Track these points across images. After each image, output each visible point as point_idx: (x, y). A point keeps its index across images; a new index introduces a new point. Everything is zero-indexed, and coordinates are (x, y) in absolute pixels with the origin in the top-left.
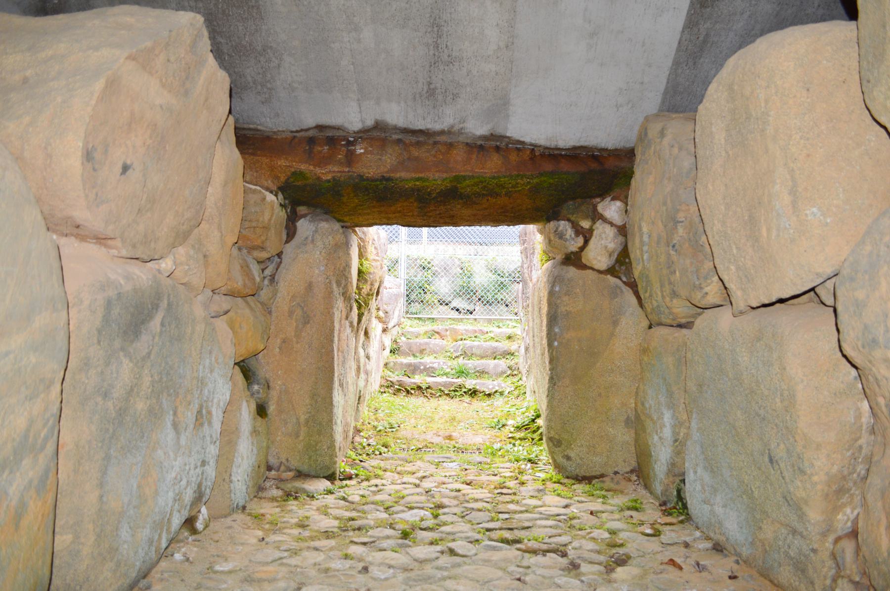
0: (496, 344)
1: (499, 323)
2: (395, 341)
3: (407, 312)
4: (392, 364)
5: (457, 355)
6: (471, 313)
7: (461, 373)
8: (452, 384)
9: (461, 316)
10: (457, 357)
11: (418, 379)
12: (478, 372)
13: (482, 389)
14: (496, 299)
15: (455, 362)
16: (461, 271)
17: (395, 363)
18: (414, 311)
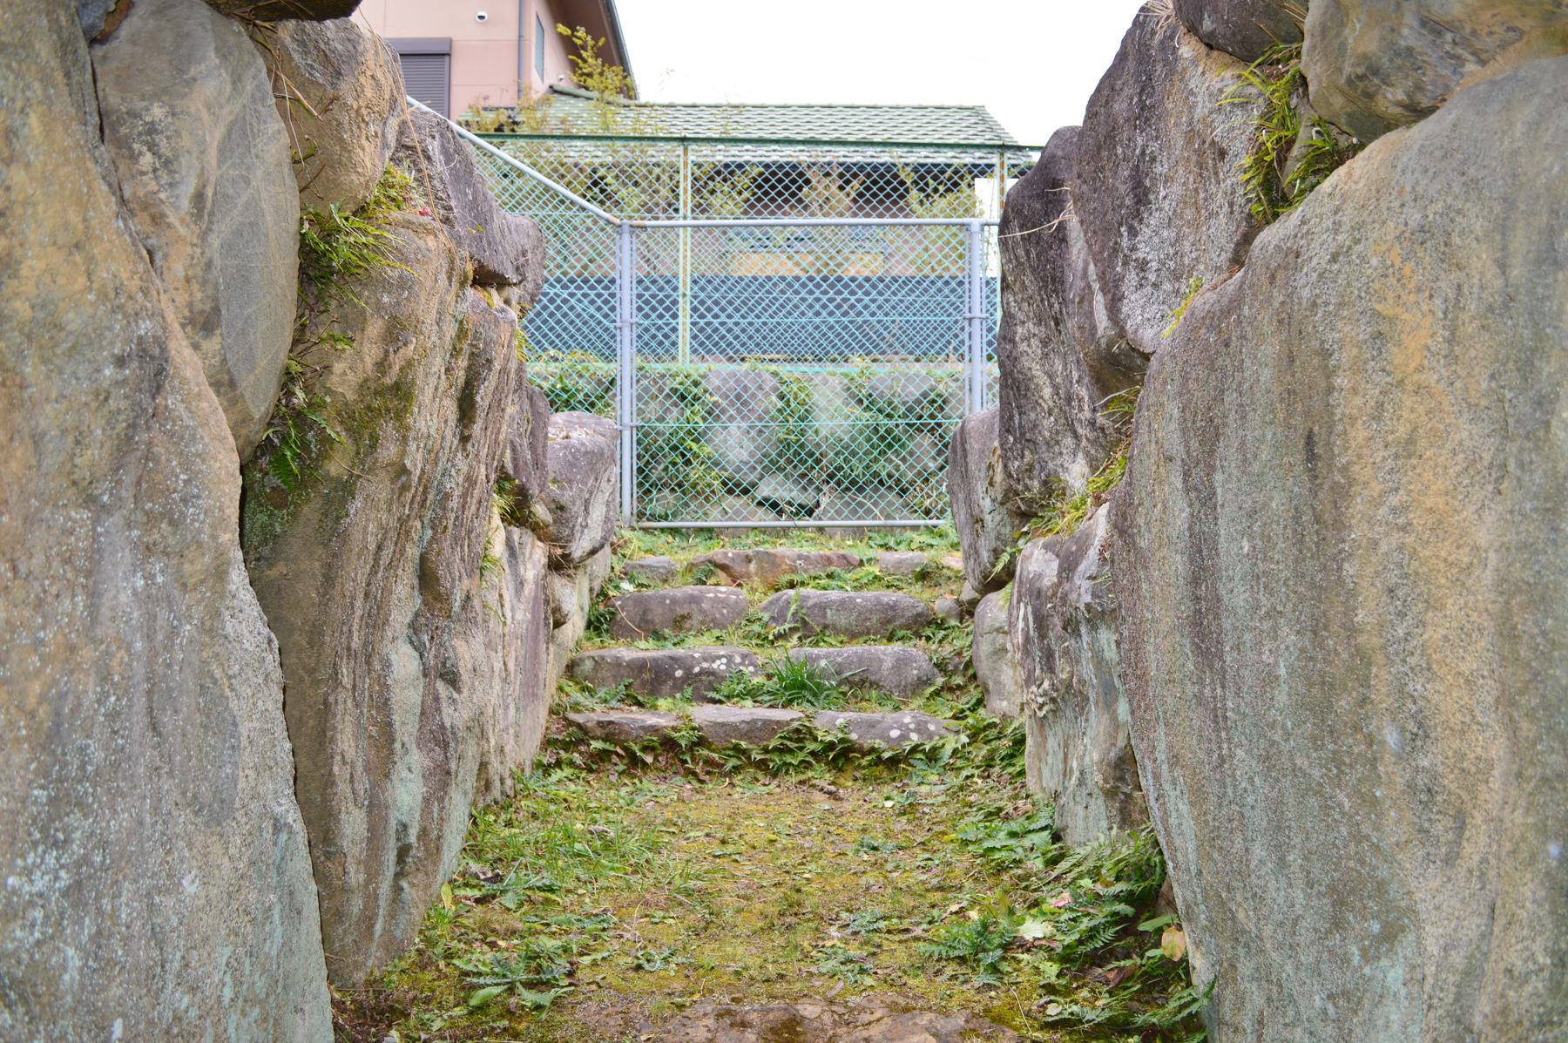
0: (890, 596)
1: (888, 536)
2: (603, 593)
3: (641, 515)
4: (589, 665)
5: (781, 629)
6: (810, 513)
7: (798, 688)
8: (771, 727)
9: (784, 522)
10: (779, 637)
11: (664, 714)
12: (847, 681)
13: (868, 743)
14: (876, 474)
15: (777, 654)
16: (780, 404)
17: (598, 663)
18: (659, 510)
